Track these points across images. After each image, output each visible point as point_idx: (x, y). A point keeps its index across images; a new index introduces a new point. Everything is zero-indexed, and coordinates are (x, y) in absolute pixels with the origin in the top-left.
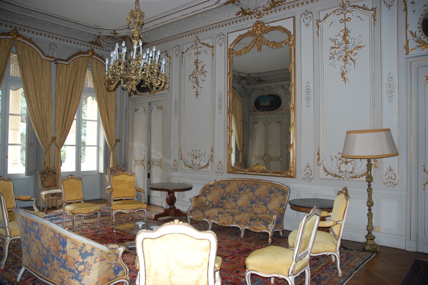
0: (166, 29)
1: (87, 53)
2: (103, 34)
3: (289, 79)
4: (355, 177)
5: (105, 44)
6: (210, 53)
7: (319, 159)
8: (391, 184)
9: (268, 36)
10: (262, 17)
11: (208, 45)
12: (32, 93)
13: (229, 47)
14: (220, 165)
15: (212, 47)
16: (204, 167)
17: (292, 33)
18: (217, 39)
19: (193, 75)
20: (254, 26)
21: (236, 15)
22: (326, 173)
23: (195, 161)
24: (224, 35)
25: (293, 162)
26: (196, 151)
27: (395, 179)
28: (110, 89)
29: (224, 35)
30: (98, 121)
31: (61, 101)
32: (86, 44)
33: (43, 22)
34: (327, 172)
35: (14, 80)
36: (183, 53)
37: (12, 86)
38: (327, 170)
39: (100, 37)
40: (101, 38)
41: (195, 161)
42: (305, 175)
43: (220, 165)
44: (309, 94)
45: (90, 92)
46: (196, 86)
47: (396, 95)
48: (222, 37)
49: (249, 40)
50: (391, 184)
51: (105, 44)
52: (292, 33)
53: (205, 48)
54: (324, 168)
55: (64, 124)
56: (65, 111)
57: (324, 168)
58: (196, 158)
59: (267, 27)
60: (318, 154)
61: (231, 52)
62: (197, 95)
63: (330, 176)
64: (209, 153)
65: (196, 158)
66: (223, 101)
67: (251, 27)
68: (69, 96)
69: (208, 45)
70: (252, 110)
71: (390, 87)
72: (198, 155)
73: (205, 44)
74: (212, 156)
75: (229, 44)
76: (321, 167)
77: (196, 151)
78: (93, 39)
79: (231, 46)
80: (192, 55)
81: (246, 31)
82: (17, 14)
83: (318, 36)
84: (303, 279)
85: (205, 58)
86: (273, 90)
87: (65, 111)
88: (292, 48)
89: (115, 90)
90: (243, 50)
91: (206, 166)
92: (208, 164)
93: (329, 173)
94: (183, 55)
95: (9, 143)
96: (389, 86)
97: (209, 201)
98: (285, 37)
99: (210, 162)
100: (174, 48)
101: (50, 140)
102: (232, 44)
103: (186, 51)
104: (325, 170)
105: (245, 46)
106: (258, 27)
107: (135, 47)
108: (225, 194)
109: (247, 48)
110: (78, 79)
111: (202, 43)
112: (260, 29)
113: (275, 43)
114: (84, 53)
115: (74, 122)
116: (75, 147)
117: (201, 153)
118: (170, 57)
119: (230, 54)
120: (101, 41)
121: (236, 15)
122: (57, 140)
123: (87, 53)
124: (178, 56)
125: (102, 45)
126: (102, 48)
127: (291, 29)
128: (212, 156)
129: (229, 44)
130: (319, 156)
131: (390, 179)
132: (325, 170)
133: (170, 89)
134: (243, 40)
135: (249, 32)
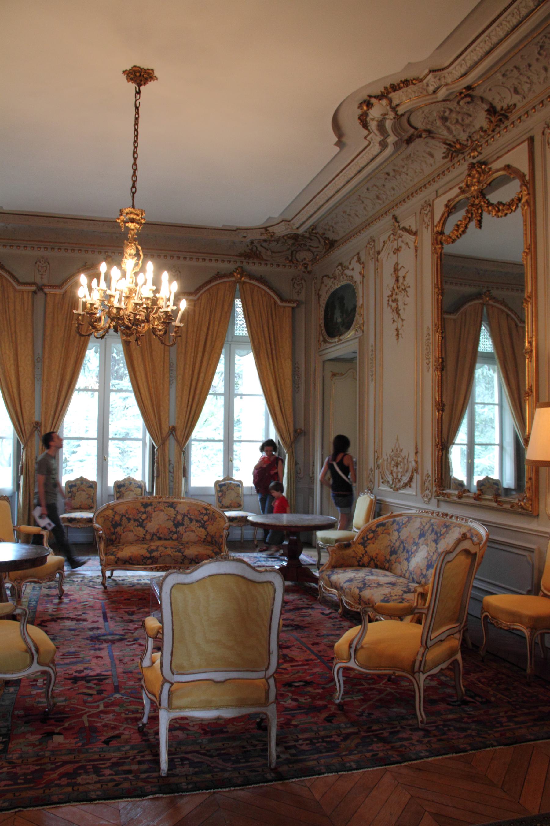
1: (231, 275)
10: (481, 153)
12: (136, 354)
15: (415, 234)
19: (391, 296)
21: (443, 158)
30: (501, 406)
31: (185, 364)
35: (240, 340)
36: (379, 253)
37: (237, 351)
45: (487, 358)
46: (395, 316)
55: (190, 404)
56: (192, 379)
61: (439, 238)
62: (398, 335)
68: (200, 354)
84: (427, 693)
87: (192, 379)
95: (222, 443)
97: (150, 533)
101: (165, 430)
108: (179, 518)
110: (217, 323)
114: (225, 276)
115: (467, 411)
116: (96, 441)
118: (363, 263)
121: (443, 158)
122: (179, 433)
123: (231, 275)
125: (265, 257)
126: (263, 262)
127: (525, 169)
133: (365, 328)
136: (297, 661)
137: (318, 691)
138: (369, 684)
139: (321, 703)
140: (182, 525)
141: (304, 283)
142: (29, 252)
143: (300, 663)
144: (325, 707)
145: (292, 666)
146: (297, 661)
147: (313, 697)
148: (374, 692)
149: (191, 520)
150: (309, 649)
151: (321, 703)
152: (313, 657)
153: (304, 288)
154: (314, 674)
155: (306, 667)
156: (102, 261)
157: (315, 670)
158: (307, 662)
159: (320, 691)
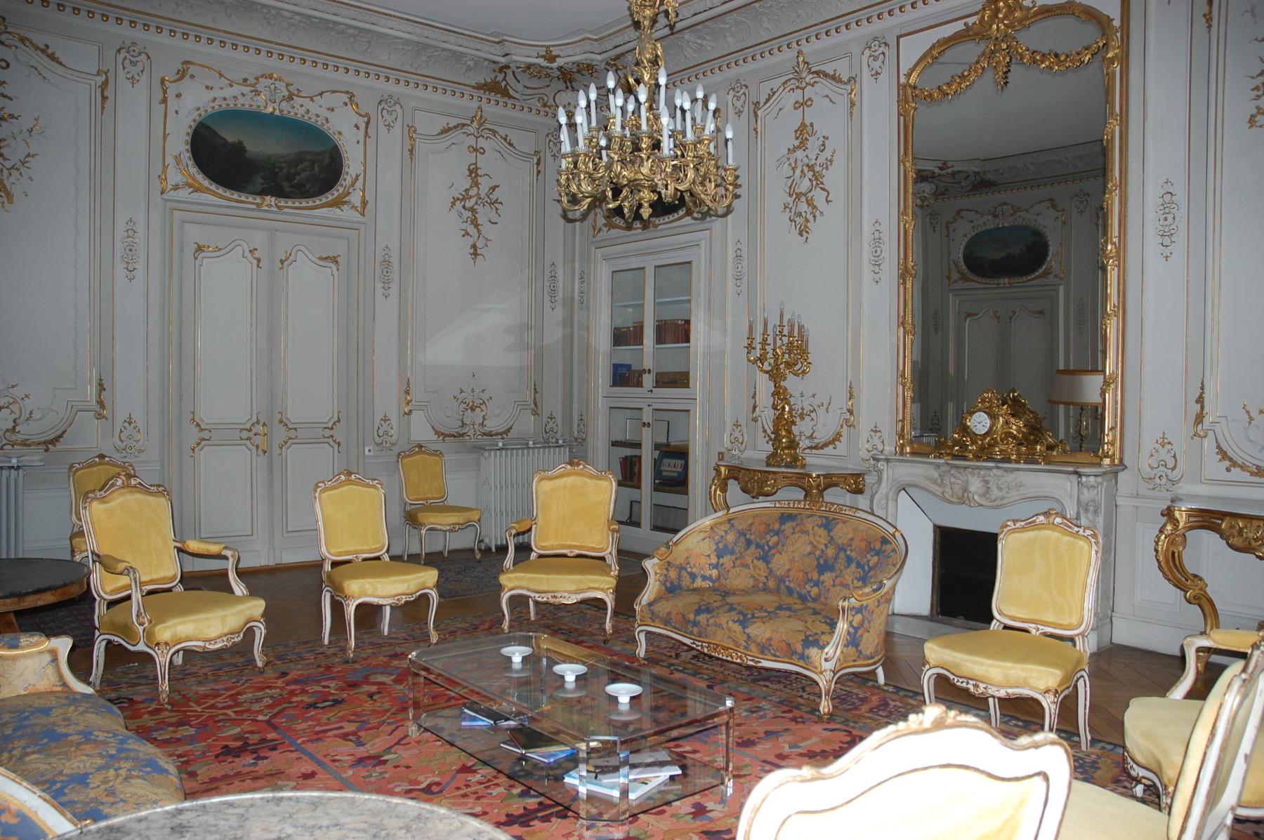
0: (700, 37)
2: (514, 58)
3: (1102, 171)
4: (816, 448)
5: (520, 87)
6: (842, 103)
7: (1199, 419)
8: (1164, 480)
9: (1030, 39)
11: (835, 78)
13: (903, 80)
14: (876, 438)
16: (826, 445)
17: (1117, 23)
18: (865, 58)
20: (984, 9)
22: (1227, 463)
23: (469, 417)
24: (886, 44)
25: (1112, 429)
26: (473, 390)
27: (1173, 469)
28: (570, 215)
29: (886, 44)
32: (468, 91)
33: (351, 31)
34: (1231, 459)
38: (1230, 453)
39: (507, 67)
40: (509, 72)
41: (469, 417)
42: (1152, 468)
43: (876, 438)
44: (1170, 217)
47: (1180, 237)
48: (881, 50)
49: (970, 51)
50: (1164, 480)
51: (520, 87)
52: (1117, 23)
53: (824, 86)
54: (1219, 447)
57: (1219, 447)
58: (473, 410)
59: (1029, 9)
60: (1200, 400)
61: (908, 96)
63: (1236, 473)
64: (841, 401)
65: (473, 410)
66: (885, 247)
67: (976, 13)
69: (835, 78)
70: (955, 275)
71: (1166, 219)
72: (478, 402)
73: (826, 75)
74: (850, 412)
75: (903, 70)
76: (1208, 445)
77: (473, 390)
78: (484, 76)
79: (908, 75)
80: (784, 111)
81: (959, 26)
82: (287, 14)
83: (1210, 27)
85: (827, 115)
86: (1023, 214)
88: (1114, 72)
89: (585, 216)
90: (949, 85)
91: (832, 442)
92: (837, 437)
93: (1234, 463)
94: (759, 113)
96: (1162, 218)
98: (1089, 34)
99: (845, 430)
100: (867, 52)
102: (913, 70)
103: (767, 100)
104: (1224, 455)
105: (958, 70)
106: (998, 10)
107: (583, 103)
109: (962, 77)
111: (817, 73)
112: (1005, 17)
113: (1057, 56)
117: (816, 401)
119: (907, 102)
120: (510, 79)
124: (745, 115)
125: (511, 92)
128: (850, 412)
129: (903, 70)
130: (1202, 408)
131: (1161, 468)
132: (1224, 455)
134: (949, 56)
135: (968, 28)
136: (335, 736)
137: (299, 699)
138: (225, 714)
139: (293, 687)
140: (832, 569)
141: (400, 111)
142: (845, 35)
143: (330, 734)
144: (288, 683)
145: (342, 728)
146: (335, 736)
147: (304, 692)
148: (221, 705)
149: (849, 560)
150: (318, 762)
151: (293, 687)
152: (310, 747)
153: (399, 119)
154: (305, 720)
155: (318, 729)
156: (73, 636)
157: (304, 726)
158: (318, 737)
159: (295, 699)
